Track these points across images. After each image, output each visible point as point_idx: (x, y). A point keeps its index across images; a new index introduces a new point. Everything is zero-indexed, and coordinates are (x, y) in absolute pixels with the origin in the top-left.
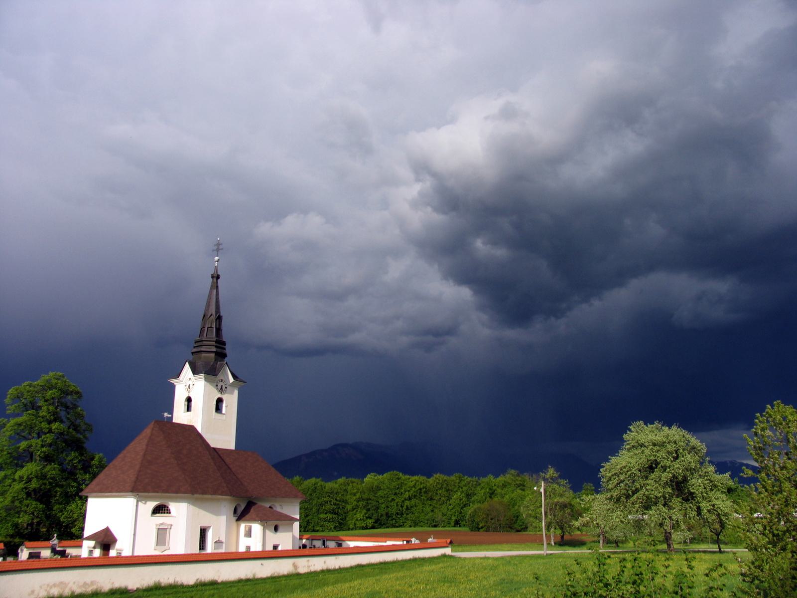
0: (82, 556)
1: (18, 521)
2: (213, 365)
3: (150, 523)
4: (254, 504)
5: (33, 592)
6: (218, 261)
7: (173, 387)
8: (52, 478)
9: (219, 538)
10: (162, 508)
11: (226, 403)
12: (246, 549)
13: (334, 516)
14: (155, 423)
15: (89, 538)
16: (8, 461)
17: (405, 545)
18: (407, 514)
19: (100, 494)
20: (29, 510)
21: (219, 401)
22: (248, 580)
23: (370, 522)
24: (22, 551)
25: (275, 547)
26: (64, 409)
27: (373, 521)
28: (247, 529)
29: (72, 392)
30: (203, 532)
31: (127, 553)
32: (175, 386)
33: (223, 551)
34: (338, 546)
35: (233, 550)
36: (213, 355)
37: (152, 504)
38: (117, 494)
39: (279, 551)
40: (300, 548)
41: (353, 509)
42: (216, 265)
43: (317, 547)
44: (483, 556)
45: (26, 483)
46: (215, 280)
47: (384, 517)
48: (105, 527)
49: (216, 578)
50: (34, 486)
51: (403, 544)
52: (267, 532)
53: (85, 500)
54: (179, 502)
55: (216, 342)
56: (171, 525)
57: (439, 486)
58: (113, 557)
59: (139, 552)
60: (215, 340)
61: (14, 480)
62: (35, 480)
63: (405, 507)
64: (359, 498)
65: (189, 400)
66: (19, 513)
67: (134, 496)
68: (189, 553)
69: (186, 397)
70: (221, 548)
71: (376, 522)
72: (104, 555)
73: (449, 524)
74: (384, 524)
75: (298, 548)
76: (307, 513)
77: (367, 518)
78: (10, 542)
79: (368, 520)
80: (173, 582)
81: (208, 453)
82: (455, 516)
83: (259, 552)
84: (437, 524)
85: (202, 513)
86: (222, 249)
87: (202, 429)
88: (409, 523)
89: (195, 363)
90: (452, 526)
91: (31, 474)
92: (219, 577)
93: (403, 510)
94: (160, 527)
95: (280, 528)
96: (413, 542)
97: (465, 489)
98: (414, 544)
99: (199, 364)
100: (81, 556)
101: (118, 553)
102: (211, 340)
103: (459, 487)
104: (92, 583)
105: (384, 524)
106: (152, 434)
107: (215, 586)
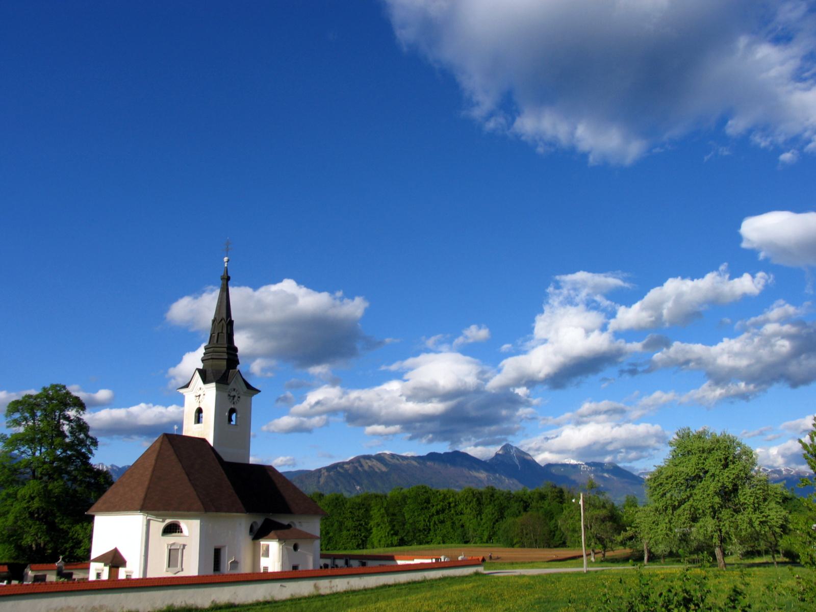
2: (225, 374)
3: (162, 544)
15: (97, 560)
23: (396, 539)
30: (217, 552)
31: (137, 574)
40: (321, 567)
45: (29, 502)
48: (113, 548)
49: (232, 601)
51: (432, 563)
53: (91, 519)
56: (184, 546)
58: (104, 581)
59: (151, 574)
83: (277, 572)
91: (33, 493)
96: (443, 560)
98: (443, 562)
99: (209, 375)
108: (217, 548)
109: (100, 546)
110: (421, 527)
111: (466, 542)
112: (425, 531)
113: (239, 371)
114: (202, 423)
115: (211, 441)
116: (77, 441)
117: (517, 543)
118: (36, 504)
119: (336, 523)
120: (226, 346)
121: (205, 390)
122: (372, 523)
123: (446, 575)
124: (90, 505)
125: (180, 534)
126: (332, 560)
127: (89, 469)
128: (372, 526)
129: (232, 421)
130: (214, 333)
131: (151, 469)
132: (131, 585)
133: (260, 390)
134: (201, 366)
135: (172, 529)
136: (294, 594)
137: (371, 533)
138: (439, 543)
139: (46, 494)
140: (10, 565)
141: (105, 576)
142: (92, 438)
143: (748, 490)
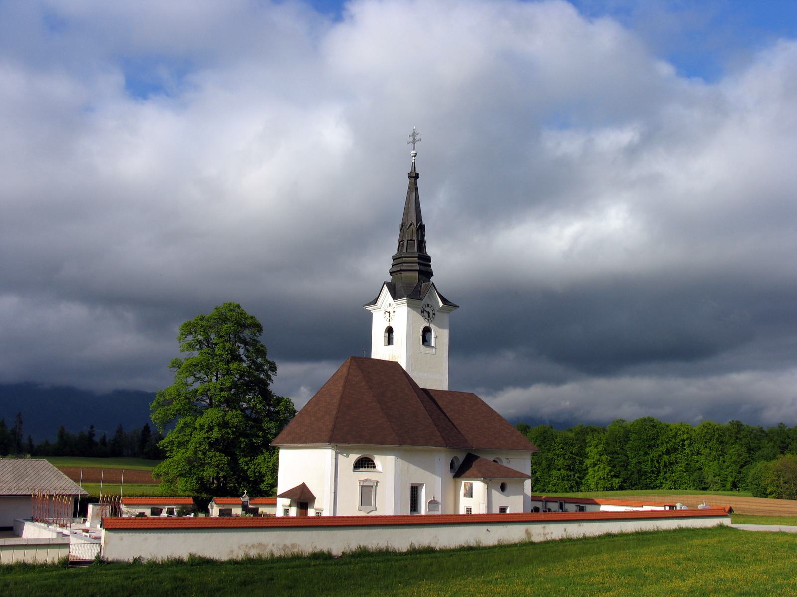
0: (278, 516)
1: (202, 475)
2: (417, 287)
3: (353, 480)
4: (477, 457)
6: (415, 156)
7: (369, 317)
8: (235, 427)
9: (434, 497)
10: (366, 461)
11: (435, 333)
12: (467, 511)
13: (569, 473)
14: (351, 360)
15: (284, 496)
16: (187, 407)
17: (667, 511)
18: (666, 473)
19: (292, 445)
20: (214, 461)
21: (427, 331)
22: (470, 548)
23: (616, 481)
24: (212, 507)
25: (503, 510)
26: (242, 346)
27: (621, 479)
28: (467, 487)
29: (250, 326)
30: (415, 491)
31: (327, 513)
32: (371, 314)
33: (439, 513)
35: (450, 512)
36: (417, 274)
37: (354, 457)
38: (313, 444)
39: (508, 514)
40: (532, 511)
41: (595, 465)
42: (413, 161)
43: (552, 510)
44: (778, 530)
45: (207, 432)
46: (413, 180)
47: (636, 476)
49: (433, 545)
50: (216, 435)
51: (665, 511)
52: (493, 491)
53: (274, 452)
54: (386, 455)
55: (419, 258)
56: (377, 482)
57: (708, 437)
58: (293, 518)
59: (341, 513)
60: (418, 255)
61: (195, 429)
62: (216, 429)
63: (662, 464)
64: (601, 451)
65: (389, 331)
66: (203, 465)
67: (332, 447)
70: (436, 509)
71: (624, 481)
72: (301, 514)
73: (723, 486)
74: (635, 484)
75: (530, 512)
76: (535, 469)
77: (612, 476)
78: (198, 497)
79: (614, 479)
80: (409, 548)
81: (416, 394)
82: (732, 476)
83: (483, 515)
84: (706, 486)
85: (413, 467)
86: (420, 140)
87: (407, 366)
88: (670, 483)
89: (395, 285)
90: (728, 490)
91: (212, 422)
92: (437, 543)
93: (659, 468)
94: (364, 485)
95: (509, 488)
96: (678, 508)
97: (744, 441)
98: (679, 511)
99: (399, 286)
101: (317, 513)
102: (413, 255)
103: (737, 438)
104: (293, 546)
105: (635, 484)
106: (348, 373)
107: (433, 555)
108: (414, 485)
110: (648, 468)
111: (705, 489)
112: (653, 473)
113: (433, 283)
114: (393, 344)
116: (254, 366)
117: (771, 493)
119: (544, 461)
121: (395, 307)
122: (588, 462)
123: (684, 527)
125: (372, 469)
126: (544, 504)
128: (588, 466)
130: (402, 241)
133: (458, 305)
134: (389, 278)
135: (363, 463)
136: (501, 538)
137: (587, 473)
138: (671, 488)
140: (195, 499)
142: (269, 362)
143: (733, 474)
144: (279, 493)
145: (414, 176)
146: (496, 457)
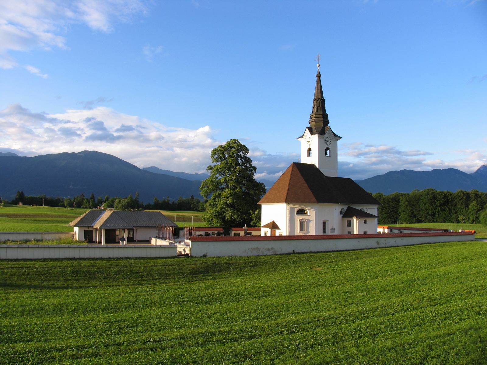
0: (262, 235)
5: (245, 251)
9: (333, 227)
15: (265, 226)
31: (284, 234)
32: (301, 142)
34: (400, 232)
36: (314, 122)
37: (297, 208)
48: (272, 221)
53: (260, 207)
68: (317, 235)
69: (312, 149)
99: (314, 129)
100: (261, 235)
104: (272, 249)
109: (265, 219)
113: (330, 127)
114: (123, 124)
115: (317, 166)
118: (230, 200)
120: (322, 114)
124: (259, 200)
127: (253, 181)
129: (327, 154)
131: (288, 181)
132: (281, 238)
135: (301, 212)
139: (235, 195)
141: (269, 234)
144: (262, 226)
145: (319, 76)
146: (362, 208)
